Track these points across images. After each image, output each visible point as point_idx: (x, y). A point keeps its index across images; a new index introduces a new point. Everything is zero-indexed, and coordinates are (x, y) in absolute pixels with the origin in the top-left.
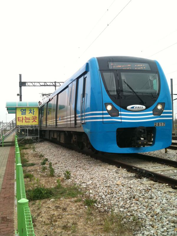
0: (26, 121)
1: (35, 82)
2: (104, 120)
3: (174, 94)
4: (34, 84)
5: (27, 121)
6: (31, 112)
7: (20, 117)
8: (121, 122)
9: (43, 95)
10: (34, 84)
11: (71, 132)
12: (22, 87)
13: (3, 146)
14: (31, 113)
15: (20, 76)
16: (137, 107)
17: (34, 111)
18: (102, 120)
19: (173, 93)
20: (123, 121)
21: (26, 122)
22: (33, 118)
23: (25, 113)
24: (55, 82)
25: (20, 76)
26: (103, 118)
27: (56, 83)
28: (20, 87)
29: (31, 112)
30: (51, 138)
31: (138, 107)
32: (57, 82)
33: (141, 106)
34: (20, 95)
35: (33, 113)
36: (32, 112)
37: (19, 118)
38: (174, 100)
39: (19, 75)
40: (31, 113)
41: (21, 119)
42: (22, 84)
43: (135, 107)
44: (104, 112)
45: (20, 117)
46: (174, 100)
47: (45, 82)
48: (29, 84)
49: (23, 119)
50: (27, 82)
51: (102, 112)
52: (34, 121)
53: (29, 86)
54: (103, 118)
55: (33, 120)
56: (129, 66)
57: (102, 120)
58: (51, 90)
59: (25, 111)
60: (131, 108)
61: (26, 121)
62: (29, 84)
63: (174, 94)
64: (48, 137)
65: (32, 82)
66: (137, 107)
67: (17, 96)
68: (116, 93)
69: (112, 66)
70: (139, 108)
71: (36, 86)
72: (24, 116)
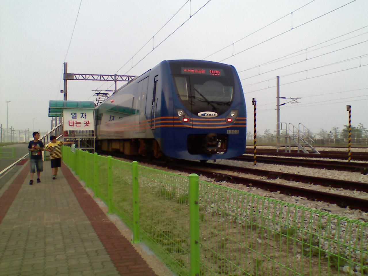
0: (76, 125)
1: (86, 75)
2: (175, 126)
3: (281, 98)
4: (85, 77)
5: (77, 125)
6: (82, 116)
7: (71, 121)
8: (193, 128)
9: (98, 94)
10: (85, 77)
11: (139, 140)
12: (68, 81)
13: (88, 132)
14: (82, 117)
15: (66, 65)
16: (209, 115)
17: (85, 116)
18: (172, 126)
19: (280, 97)
20: (194, 127)
21: (76, 126)
22: (85, 122)
23: (76, 117)
24: (116, 76)
25: (66, 65)
26: (174, 124)
27: (117, 77)
28: (65, 80)
29: (82, 116)
30: (110, 150)
31: (210, 115)
32: (119, 76)
33: (214, 113)
34: (65, 92)
35: (84, 117)
36: (84, 115)
37: (70, 122)
38: (281, 105)
39: (64, 64)
40: (82, 117)
41: (72, 122)
42: (68, 77)
43: (206, 115)
44: (175, 117)
45: (71, 121)
46: (281, 105)
47: (100, 75)
48: (77, 76)
49: (73, 123)
50: (75, 74)
51: (173, 117)
52: (87, 125)
53: (78, 79)
54: (174, 124)
55: (86, 124)
56: (202, 71)
57: (172, 126)
58: (109, 86)
59: (76, 115)
60: (201, 115)
61: (76, 125)
62: (77, 76)
63: (281, 98)
64: (75, 77)
65: (81, 75)
66: (209, 115)
67: (60, 91)
68: (187, 99)
69: (185, 70)
70: (211, 115)
71: (87, 80)
72: (75, 120)
